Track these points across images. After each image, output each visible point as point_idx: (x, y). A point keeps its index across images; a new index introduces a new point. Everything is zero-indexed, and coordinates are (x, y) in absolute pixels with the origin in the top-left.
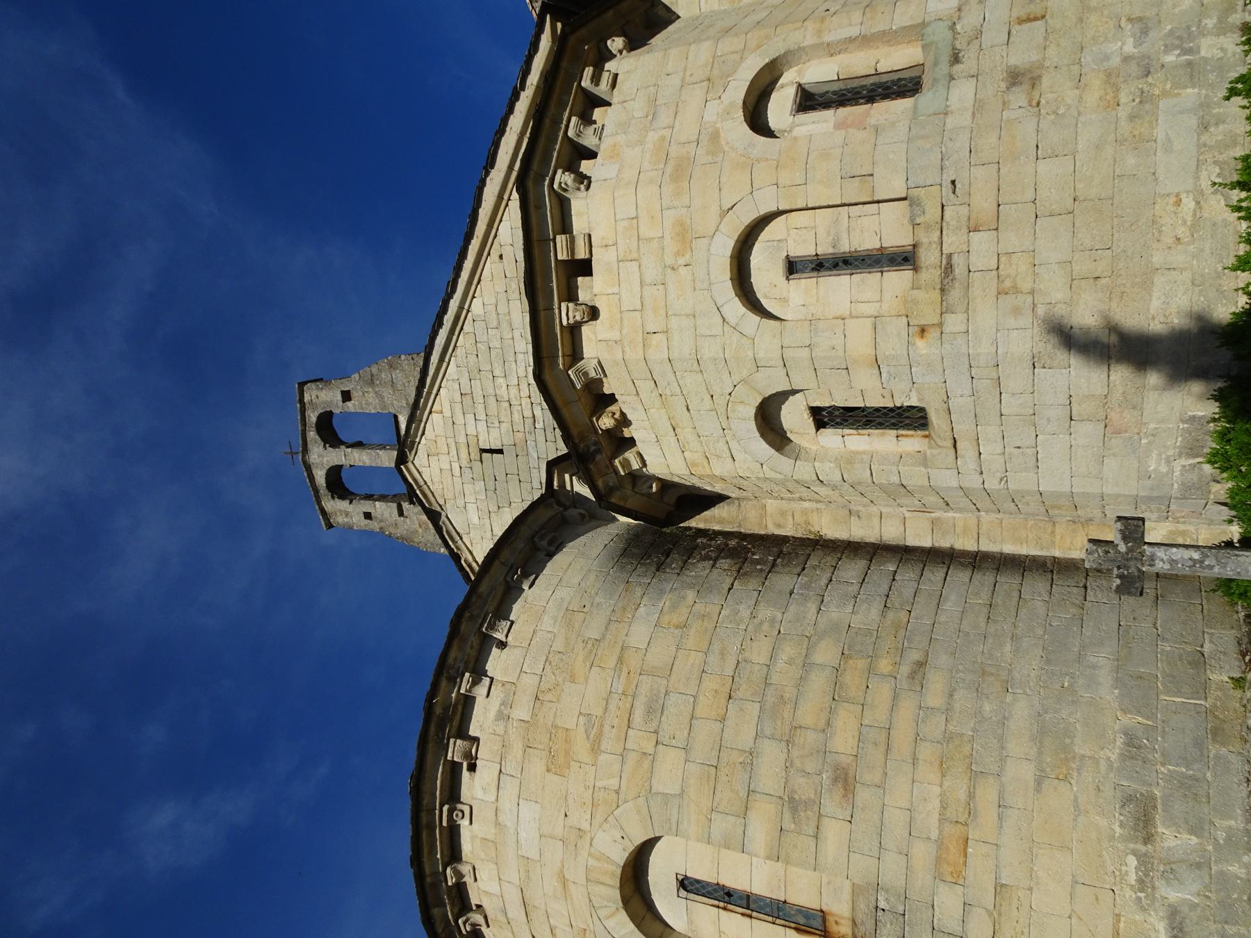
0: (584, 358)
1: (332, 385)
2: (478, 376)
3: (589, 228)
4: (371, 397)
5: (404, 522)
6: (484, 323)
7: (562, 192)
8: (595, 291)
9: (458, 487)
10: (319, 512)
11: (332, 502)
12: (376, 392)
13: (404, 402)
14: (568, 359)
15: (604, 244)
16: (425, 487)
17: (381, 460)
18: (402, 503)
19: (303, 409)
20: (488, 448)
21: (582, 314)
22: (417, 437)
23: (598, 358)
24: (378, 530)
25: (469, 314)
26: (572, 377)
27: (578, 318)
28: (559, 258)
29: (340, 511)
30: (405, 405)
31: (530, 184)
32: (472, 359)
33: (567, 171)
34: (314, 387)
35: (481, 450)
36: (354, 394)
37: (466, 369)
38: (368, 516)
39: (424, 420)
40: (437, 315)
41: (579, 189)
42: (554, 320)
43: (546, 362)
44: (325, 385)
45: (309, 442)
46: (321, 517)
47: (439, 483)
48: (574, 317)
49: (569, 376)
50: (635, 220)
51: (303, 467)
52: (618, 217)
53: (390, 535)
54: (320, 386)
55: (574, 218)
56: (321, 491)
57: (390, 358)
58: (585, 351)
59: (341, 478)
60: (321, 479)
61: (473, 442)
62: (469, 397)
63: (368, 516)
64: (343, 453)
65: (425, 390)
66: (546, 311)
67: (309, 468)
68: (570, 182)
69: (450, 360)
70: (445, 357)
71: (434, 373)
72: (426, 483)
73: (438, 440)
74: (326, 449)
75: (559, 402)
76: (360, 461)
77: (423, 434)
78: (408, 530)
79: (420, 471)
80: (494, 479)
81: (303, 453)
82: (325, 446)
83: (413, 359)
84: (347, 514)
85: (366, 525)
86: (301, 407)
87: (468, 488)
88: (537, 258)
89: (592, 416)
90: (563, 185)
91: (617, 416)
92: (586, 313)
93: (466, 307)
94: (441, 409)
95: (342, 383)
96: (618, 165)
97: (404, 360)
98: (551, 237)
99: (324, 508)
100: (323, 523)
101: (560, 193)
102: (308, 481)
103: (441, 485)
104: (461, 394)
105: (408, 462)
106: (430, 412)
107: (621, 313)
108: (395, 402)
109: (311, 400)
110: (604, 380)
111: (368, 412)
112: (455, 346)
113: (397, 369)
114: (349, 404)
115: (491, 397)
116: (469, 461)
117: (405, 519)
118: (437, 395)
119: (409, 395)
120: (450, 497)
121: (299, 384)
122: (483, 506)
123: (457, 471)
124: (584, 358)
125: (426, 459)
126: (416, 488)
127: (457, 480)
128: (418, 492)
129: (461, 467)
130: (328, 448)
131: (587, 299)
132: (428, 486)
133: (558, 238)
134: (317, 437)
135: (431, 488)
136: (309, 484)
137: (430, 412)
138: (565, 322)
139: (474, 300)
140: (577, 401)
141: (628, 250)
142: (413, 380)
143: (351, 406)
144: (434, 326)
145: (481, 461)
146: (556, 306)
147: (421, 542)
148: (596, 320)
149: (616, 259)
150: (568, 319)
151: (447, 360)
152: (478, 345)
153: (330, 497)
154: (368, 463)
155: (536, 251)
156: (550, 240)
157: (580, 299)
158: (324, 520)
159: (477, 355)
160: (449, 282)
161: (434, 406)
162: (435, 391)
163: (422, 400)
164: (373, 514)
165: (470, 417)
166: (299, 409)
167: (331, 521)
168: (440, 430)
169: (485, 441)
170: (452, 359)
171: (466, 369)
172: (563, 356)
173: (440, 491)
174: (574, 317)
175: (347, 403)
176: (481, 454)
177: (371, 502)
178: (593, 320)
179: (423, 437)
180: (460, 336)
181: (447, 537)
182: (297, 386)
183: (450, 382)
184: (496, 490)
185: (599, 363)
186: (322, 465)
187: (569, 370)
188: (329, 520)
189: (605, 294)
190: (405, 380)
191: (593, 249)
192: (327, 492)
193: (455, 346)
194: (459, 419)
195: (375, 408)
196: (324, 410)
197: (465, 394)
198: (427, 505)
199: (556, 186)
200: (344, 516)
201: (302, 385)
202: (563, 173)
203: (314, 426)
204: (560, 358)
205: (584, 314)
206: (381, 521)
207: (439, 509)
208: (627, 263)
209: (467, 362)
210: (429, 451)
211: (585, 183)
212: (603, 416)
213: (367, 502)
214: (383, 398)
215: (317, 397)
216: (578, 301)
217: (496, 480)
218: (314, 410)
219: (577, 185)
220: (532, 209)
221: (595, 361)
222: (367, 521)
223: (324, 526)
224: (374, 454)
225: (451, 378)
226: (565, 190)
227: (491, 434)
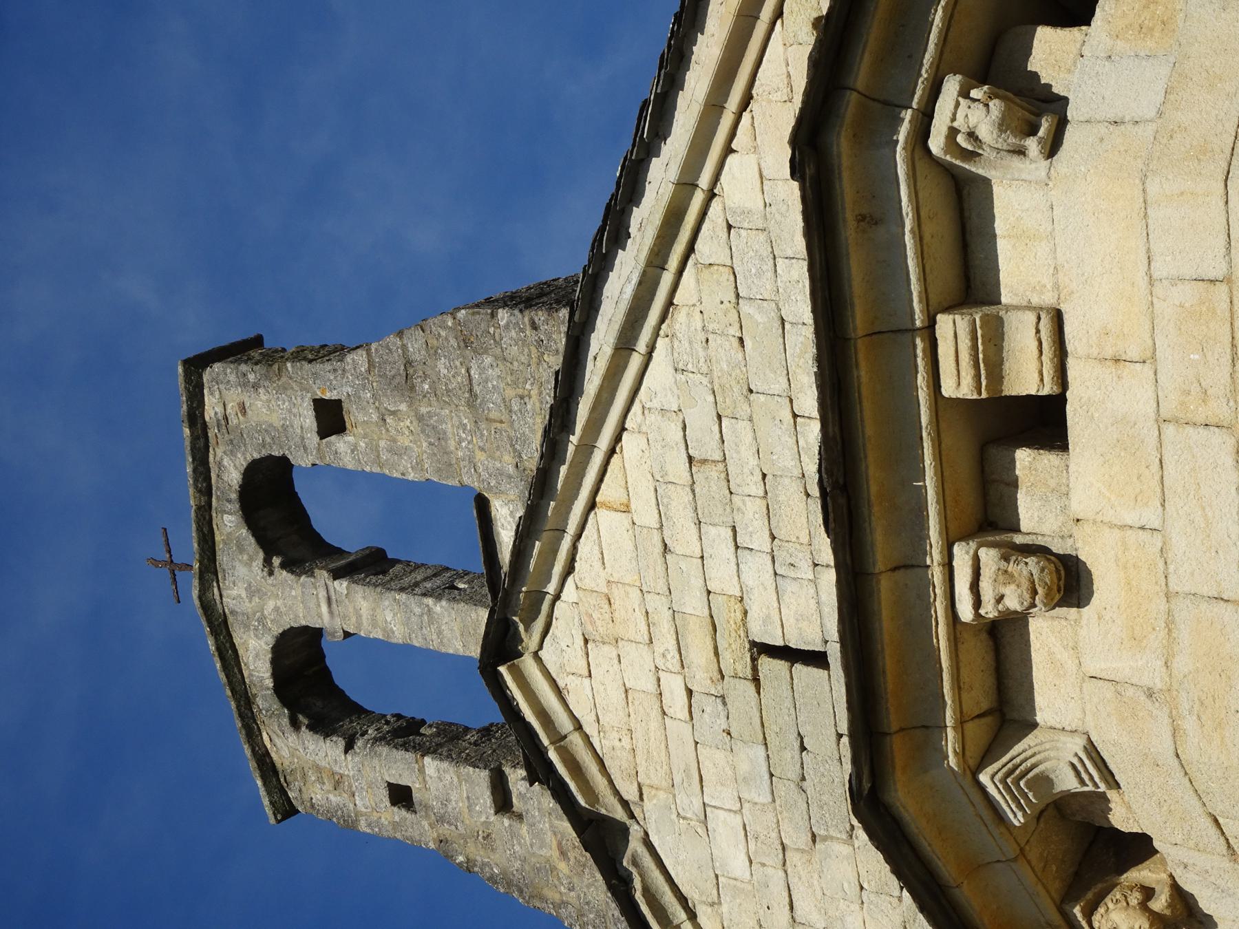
0: (1034, 725)
1: (284, 379)
2: (743, 411)
3: (1056, 287)
4: (404, 429)
5: (514, 834)
6: (762, 237)
7: (958, 162)
8: (1078, 506)
9: (683, 754)
10: (252, 765)
11: (292, 738)
12: (420, 418)
13: (508, 460)
14: (978, 731)
15: (1109, 352)
16: (576, 740)
17: (440, 633)
18: (507, 770)
19: (201, 443)
20: (780, 643)
21: (1027, 596)
22: (548, 579)
23: (1087, 733)
24: (432, 845)
25: (716, 205)
26: (992, 790)
27: (1013, 603)
28: (948, 389)
29: (318, 769)
30: (511, 469)
31: (843, 146)
32: (724, 349)
33: (982, 81)
34: (232, 378)
35: (753, 644)
36: (353, 415)
37: (705, 381)
38: (401, 796)
39: (572, 528)
40: (608, 207)
41: (1021, 152)
42: (928, 606)
43: (898, 748)
44: (267, 378)
45: (220, 546)
46: (259, 783)
47: (619, 730)
48: (1000, 599)
49: (982, 789)
50: (1223, 288)
51: (204, 623)
52: (1159, 269)
53: (469, 867)
54: (251, 377)
55: (1003, 246)
56: (259, 701)
57: (462, 314)
58: (1040, 700)
59: (322, 656)
60: (259, 664)
61: (727, 616)
62: (714, 472)
63: (401, 796)
64: (322, 594)
65: (574, 439)
66: (899, 574)
67: (220, 626)
68: (986, 132)
69: (651, 349)
70: (635, 338)
71: (601, 388)
72: (579, 727)
73: (616, 594)
74: (271, 573)
75: (948, 869)
76: (374, 624)
77: (569, 569)
78: (524, 860)
79: (561, 684)
80: (797, 745)
81: (201, 578)
82: (267, 562)
83: (534, 327)
84: (338, 782)
85: (395, 825)
86: (194, 438)
87: (714, 761)
88: (865, 391)
89: (1071, 893)
90: (960, 139)
91: (1160, 903)
92: (1040, 590)
93: (704, 181)
94: (624, 500)
95: (316, 376)
96: (1165, 71)
97: (507, 326)
98: (918, 323)
99: (267, 753)
100: (266, 802)
101: (951, 164)
102: (218, 665)
103: (626, 741)
104: (690, 459)
105: (520, 655)
106: (592, 506)
107: (1168, 596)
108: (480, 456)
109: (226, 418)
110: (1112, 795)
111: (396, 475)
112: (670, 303)
113: (486, 351)
114: (340, 444)
115: (787, 481)
116: (717, 676)
117: (516, 824)
118: (612, 452)
119: (525, 441)
120: (655, 782)
121: (187, 363)
122: (762, 824)
123: (676, 702)
124: (1034, 725)
125: (580, 653)
126: (546, 742)
127: (679, 729)
128: (553, 755)
129: (690, 693)
130: (277, 571)
131: (1045, 529)
132: (587, 738)
133: (945, 323)
134: (244, 532)
135: (595, 742)
136: (222, 676)
137: (592, 506)
138: (966, 612)
139: (731, 159)
140: (1015, 860)
141: (1195, 389)
142: (534, 393)
143: (343, 448)
144: (597, 241)
145: (756, 680)
146: (935, 556)
147: (564, 904)
148: (1079, 606)
149: (1151, 409)
150: (977, 603)
151: (642, 346)
152: (745, 307)
153: (285, 721)
154: (399, 634)
155: (864, 374)
156: (913, 331)
157: (1025, 525)
158: (269, 793)
159: (741, 340)
160: (645, 104)
161: (603, 486)
162: (604, 442)
163: (563, 470)
164: (416, 796)
165: (719, 537)
166: (187, 443)
167: (291, 795)
168: (622, 566)
169: (767, 620)
170: (660, 343)
171: (705, 381)
172: (961, 723)
173: (625, 755)
174: (1000, 599)
175: (333, 438)
176: (754, 660)
177: (410, 756)
178: (1070, 605)
179: (570, 580)
180: (685, 274)
181: (645, 909)
182: (180, 370)
183: (652, 418)
184: (803, 779)
185: (1092, 750)
186: (261, 620)
187: (981, 766)
188: (284, 793)
189: (1112, 526)
190: (510, 393)
191: (1071, 362)
192: (276, 705)
193: (670, 303)
194: (684, 539)
195: (418, 466)
196: (264, 453)
197: (704, 461)
198: (582, 802)
199: (936, 144)
200: (328, 786)
201: (197, 365)
202: (965, 93)
203: (234, 496)
204: (950, 733)
205: (1034, 592)
206: (441, 819)
207: (619, 814)
208: (1190, 429)
209: (708, 360)
210: (589, 628)
211: (1041, 133)
212: (1108, 900)
213: (400, 754)
214: (441, 437)
215: (243, 409)
216: (1017, 530)
217: (803, 748)
218: (233, 448)
219: (1012, 140)
220: (849, 231)
221: (1076, 745)
222: (399, 814)
223: (269, 811)
224: (417, 610)
225: (655, 404)
226: (970, 156)
227: (786, 598)
